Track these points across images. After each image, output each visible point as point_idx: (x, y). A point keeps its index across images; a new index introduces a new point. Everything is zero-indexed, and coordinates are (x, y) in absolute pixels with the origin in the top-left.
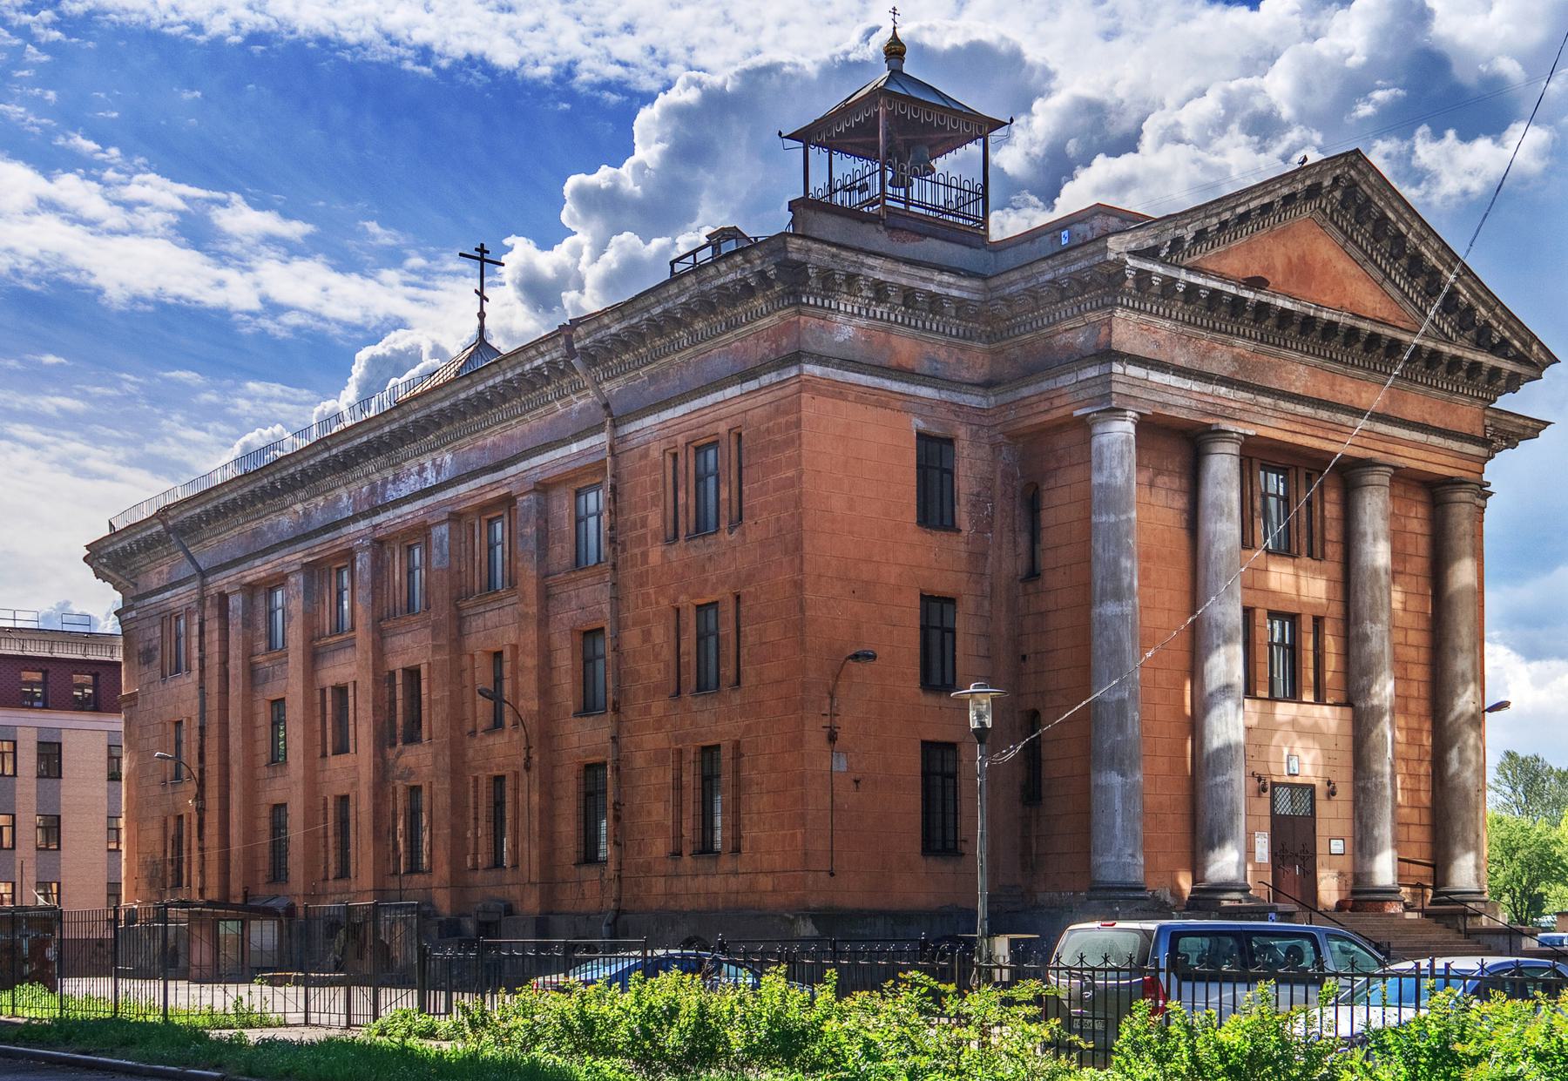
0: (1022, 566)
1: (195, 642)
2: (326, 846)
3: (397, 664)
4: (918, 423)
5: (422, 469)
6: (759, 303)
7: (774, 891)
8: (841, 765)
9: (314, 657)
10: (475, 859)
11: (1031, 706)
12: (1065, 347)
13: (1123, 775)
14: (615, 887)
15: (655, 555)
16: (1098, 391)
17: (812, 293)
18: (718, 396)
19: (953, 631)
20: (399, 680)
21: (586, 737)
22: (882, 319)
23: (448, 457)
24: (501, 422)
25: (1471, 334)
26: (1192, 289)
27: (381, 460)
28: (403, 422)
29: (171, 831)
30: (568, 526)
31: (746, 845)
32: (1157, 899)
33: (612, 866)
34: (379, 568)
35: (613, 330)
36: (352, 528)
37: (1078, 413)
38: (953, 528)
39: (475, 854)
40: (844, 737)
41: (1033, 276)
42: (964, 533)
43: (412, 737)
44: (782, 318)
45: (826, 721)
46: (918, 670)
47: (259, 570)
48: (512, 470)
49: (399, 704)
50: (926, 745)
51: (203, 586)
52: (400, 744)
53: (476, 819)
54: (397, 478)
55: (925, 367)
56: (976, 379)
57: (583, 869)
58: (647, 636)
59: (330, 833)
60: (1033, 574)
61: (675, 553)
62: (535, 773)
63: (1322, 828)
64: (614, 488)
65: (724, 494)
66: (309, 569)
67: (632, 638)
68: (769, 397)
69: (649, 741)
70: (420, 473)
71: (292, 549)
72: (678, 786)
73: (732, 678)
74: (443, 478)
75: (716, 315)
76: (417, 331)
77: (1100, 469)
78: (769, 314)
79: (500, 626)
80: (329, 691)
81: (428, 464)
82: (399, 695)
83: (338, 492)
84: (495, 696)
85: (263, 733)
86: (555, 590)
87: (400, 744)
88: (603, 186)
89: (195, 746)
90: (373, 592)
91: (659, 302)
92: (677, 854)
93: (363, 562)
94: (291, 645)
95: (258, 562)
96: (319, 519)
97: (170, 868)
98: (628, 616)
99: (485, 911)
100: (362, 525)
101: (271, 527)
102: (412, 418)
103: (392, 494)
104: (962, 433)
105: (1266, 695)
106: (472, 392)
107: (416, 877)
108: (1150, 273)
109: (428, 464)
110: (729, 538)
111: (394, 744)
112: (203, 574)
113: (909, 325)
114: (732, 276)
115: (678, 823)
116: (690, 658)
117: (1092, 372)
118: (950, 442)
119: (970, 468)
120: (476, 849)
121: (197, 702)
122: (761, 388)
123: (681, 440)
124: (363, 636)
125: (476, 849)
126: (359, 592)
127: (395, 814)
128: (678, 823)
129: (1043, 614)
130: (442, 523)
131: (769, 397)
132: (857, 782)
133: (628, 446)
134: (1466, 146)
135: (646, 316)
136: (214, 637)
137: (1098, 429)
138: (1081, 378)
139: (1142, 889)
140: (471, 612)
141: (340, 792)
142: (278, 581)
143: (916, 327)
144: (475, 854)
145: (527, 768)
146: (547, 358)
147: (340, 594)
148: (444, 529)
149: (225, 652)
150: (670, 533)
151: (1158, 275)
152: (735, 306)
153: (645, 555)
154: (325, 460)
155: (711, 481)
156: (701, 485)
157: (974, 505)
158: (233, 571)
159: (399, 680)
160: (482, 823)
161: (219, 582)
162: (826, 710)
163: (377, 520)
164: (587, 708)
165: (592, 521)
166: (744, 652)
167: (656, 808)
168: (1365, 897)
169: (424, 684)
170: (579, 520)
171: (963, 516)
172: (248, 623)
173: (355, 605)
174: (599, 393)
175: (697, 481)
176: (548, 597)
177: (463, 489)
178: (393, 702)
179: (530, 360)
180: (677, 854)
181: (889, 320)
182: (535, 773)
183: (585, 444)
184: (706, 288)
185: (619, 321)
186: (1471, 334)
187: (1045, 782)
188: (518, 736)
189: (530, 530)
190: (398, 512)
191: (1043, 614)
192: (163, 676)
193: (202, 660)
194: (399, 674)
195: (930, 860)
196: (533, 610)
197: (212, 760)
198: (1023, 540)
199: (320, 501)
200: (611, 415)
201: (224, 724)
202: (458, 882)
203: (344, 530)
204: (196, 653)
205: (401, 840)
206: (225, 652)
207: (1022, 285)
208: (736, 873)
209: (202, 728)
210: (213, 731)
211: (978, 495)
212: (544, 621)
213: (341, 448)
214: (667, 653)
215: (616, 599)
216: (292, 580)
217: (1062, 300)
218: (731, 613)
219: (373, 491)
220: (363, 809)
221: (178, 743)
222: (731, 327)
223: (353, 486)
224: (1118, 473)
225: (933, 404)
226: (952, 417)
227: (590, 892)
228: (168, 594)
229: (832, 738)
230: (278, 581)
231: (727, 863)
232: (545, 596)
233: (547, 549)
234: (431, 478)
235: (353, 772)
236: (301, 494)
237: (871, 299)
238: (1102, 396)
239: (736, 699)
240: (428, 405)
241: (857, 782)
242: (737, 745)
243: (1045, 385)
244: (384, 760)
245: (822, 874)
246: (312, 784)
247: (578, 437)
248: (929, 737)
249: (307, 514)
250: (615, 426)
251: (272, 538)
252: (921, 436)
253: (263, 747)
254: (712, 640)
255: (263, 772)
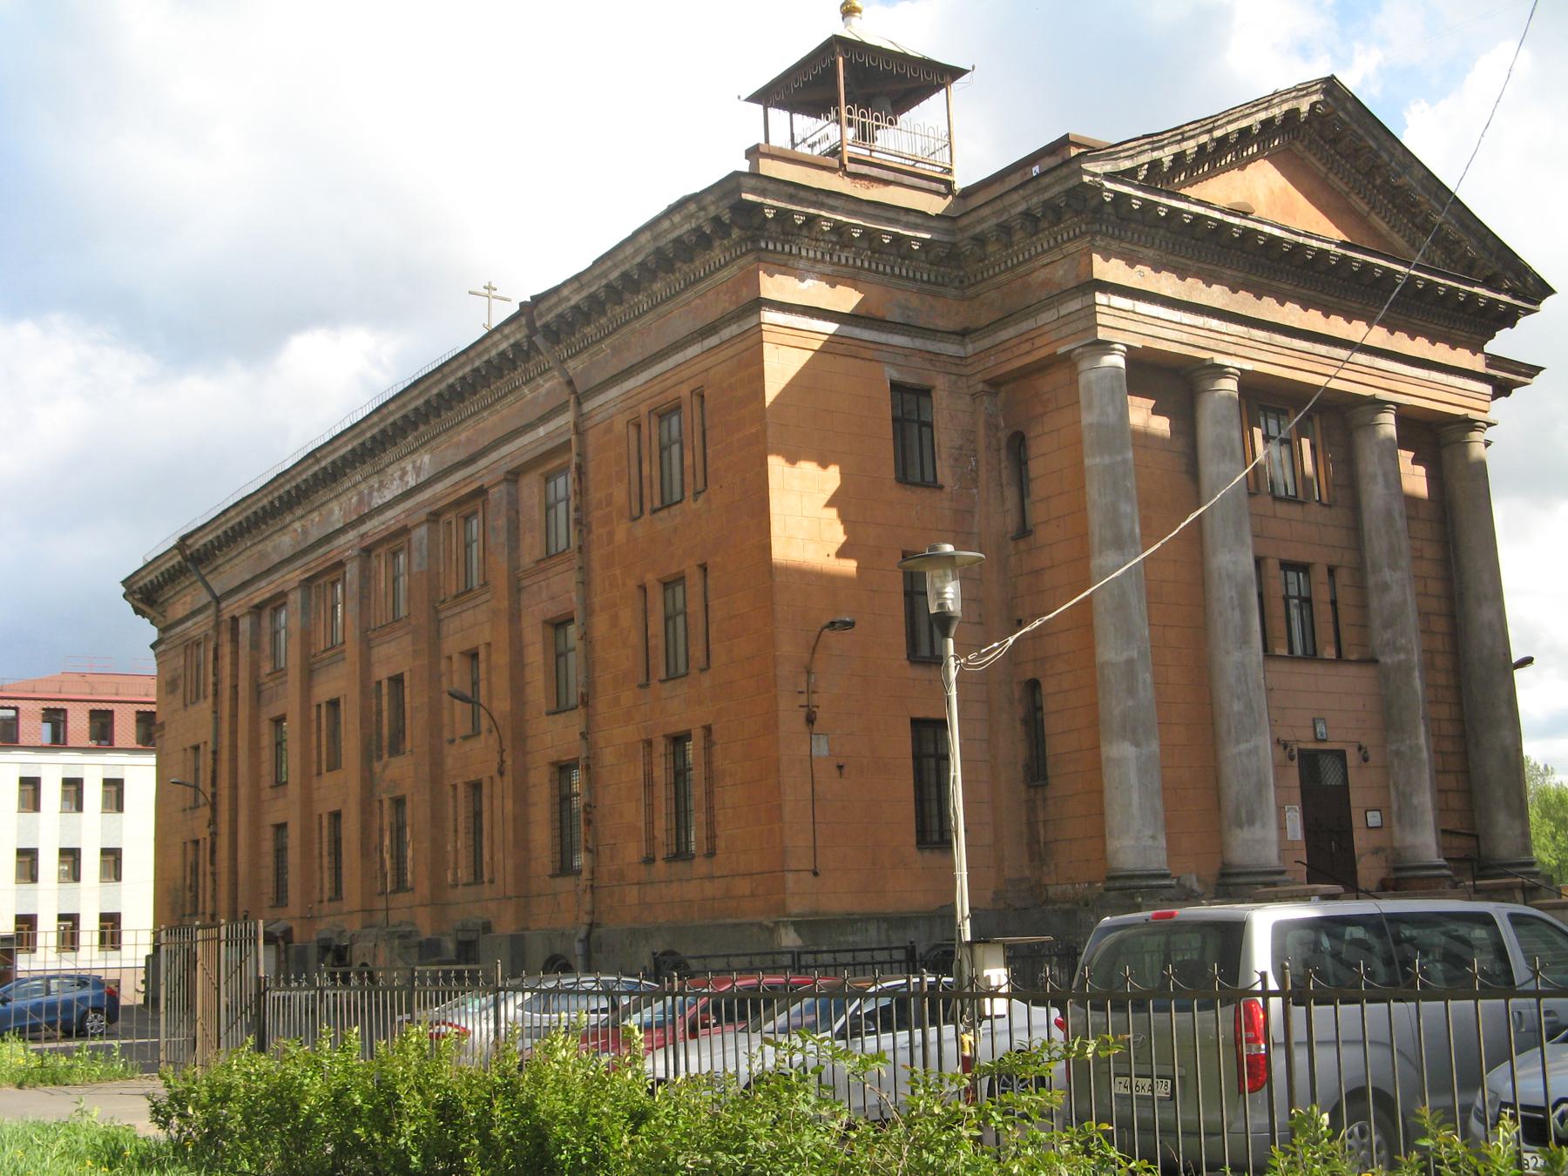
0: (1011, 522)
1: (210, 667)
2: (321, 867)
3: (382, 673)
4: (892, 374)
5: (404, 473)
6: (717, 254)
7: (753, 895)
8: (821, 748)
9: (309, 673)
10: (455, 874)
11: (1030, 676)
12: (1045, 283)
13: (1137, 745)
14: (588, 897)
15: (620, 535)
16: (1081, 325)
17: (770, 238)
18: (679, 358)
19: (930, 425)
20: (385, 690)
21: (556, 736)
22: (846, 265)
23: (426, 458)
24: (473, 414)
25: (602, 295)
26: (839, 228)
27: (368, 469)
28: (382, 425)
29: (190, 858)
30: (537, 514)
31: (721, 844)
32: (1183, 886)
33: (586, 875)
34: (366, 576)
35: (573, 302)
36: (342, 540)
37: (1061, 350)
38: (935, 485)
39: (456, 869)
40: (821, 716)
41: (1005, 209)
42: (947, 489)
43: (396, 748)
44: (741, 268)
45: (803, 700)
46: (903, 640)
47: (263, 591)
48: (483, 463)
49: (385, 714)
50: (915, 722)
51: (218, 611)
52: (386, 756)
53: (456, 831)
54: (382, 485)
55: (895, 315)
56: (951, 327)
57: (558, 880)
58: (614, 621)
59: (325, 853)
60: (1024, 531)
61: (640, 529)
62: (508, 778)
63: (1356, 798)
64: (579, 468)
65: (688, 461)
66: (307, 583)
67: (600, 624)
68: (730, 352)
69: (617, 737)
70: (401, 478)
71: (290, 568)
72: (649, 783)
73: (703, 664)
74: (422, 479)
75: (673, 272)
76: (55, 885)
77: (1090, 407)
78: (726, 264)
79: (472, 625)
80: (456, 657)
81: (409, 468)
82: (385, 705)
83: (330, 505)
84: (471, 700)
85: (267, 755)
86: (525, 583)
87: (386, 756)
88: (832, 478)
89: (209, 770)
90: (361, 603)
91: (616, 266)
92: (649, 860)
93: (352, 571)
94: (290, 664)
95: (263, 583)
96: (315, 535)
97: (188, 895)
98: (597, 601)
99: (464, 930)
100: (351, 535)
101: (274, 548)
102: (391, 420)
103: (377, 501)
104: (940, 383)
105: (1285, 652)
106: (443, 386)
107: (400, 895)
108: (1129, 196)
109: (409, 468)
110: (694, 506)
111: (380, 758)
112: (218, 600)
113: (877, 271)
114: (687, 227)
115: (650, 823)
116: (658, 642)
117: (1074, 305)
118: (925, 392)
119: (950, 415)
120: (456, 863)
121: (210, 727)
122: (722, 343)
123: (644, 409)
124: (352, 650)
125: (456, 863)
126: (348, 606)
127: (381, 829)
128: (650, 823)
129: (1037, 573)
130: (419, 525)
131: (730, 352)
132: (840, 767)
133: (589, 424)
134: (548, 955)
135: (604, 282)
136: (226, 661)
137: (1084, 365)
138: (1062, 313)
139: (1165, 876)
140: (449, 613)
141: (333, 809)
142: (277, 602)
143: (884, 273)
144: (456, 869)
145: (501, 773)
146: (512, 341)
147: (334, 608)
148: (422, 532)
149: (235, 676)
150: (636, 511)
151: (1137, 198)
152: (692, 260)
153: (611, 534)
154: (315, 474)
155: (676, 449)
156: (666, 454)
157: (956, 460)
158: (241, 595)
159: (385, 690)
160: (462, 835)
161: (231, 607)
162: (804, 688)
163: (364, 529)
164: (559, 708)
165: (562, 507)
166: (712, 628)
167: (626, 805)
168: (1410, 874)
169: (407, 692)
170: (549, 508)
171: (945, 474)
172: (255, 645)
173: (345, 613)
174: (564, 372)
175: (662, 450)
176: (520, 590)
177: (439, 487)
178: (379, 713)
179: (495, 344)
180: (649, 860)
181: (854, 266)
182: (508, 778)
183: (552, 426)
184: (661, 243)
185: (577, 291)
186: (602, 295)
187: (1050, 761)
188: (493, 740)
189: (502, 522)
190: (382, 518)
191: (1037, 573)
192: (185, 706)
193: (216, 684)
194: (385, 683)
195: (927, 853)
196: (505, 604)
197: (224, 794)
198: (1011, 494)
199: (315, 516)
200: (575, 392)
201: (234, 747)
202: (438, 902)
203: (336, 543)
204: (211, 679)
205: (387, 856)
206: (235, 676)
207: (993, 221)
208: (711, 878)
209: (215, 753)
210: (225, 755)
211: (961, 448)
212: (515, 616)
213: (330, 459)
214: (635, 638)
215: (585, 584)
216: (291, 597)
217: (1036, 233)
218: (699, 589)
219: (361, 501)
220: (418, 812)
221: (197, 770)
222: (691, 284)
223: (344, 498)
224: (1110, 410)
225: (909, 353)
226: (928, 366)
227: (562, 908)
228: (189, 623)
229: (810, 720)
230: (277, 602)
231: (701, 866)
232: (516, 589)
233: (518, 540)
234: (412, 481)
235: (340, 789)
236: (299, 512)
237: (834, 244)
238: (1085, 330)
239: (706, 681)
240: (404, 405)
241: (840, 767)
242: (708, 729)
243: (1025, 326)
244: (371, 772)
245: (803, 874)
246: (307, 802)
247: (544, 419)
248: (920, 714)
249: (305, 532)
250: (579, 404)
251: (276, 559)
252: (895, 386)
253: (267, 768)
254: (680, 619)
255: (267, 793)
